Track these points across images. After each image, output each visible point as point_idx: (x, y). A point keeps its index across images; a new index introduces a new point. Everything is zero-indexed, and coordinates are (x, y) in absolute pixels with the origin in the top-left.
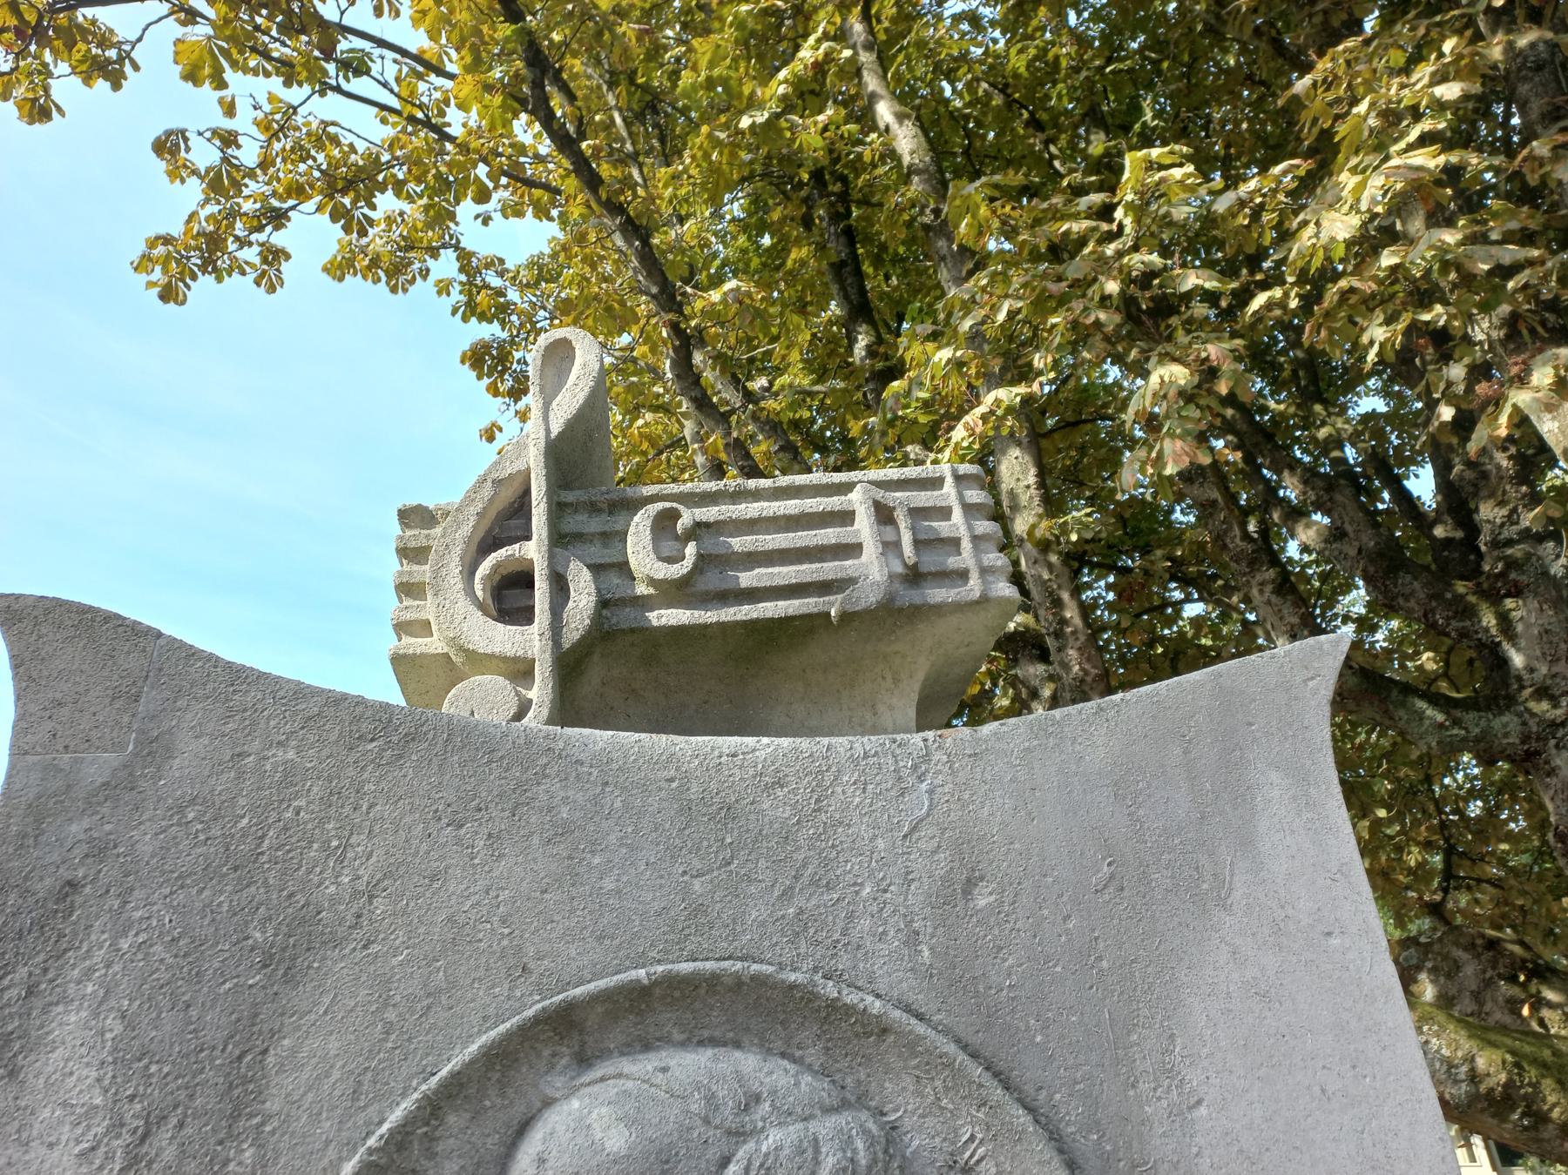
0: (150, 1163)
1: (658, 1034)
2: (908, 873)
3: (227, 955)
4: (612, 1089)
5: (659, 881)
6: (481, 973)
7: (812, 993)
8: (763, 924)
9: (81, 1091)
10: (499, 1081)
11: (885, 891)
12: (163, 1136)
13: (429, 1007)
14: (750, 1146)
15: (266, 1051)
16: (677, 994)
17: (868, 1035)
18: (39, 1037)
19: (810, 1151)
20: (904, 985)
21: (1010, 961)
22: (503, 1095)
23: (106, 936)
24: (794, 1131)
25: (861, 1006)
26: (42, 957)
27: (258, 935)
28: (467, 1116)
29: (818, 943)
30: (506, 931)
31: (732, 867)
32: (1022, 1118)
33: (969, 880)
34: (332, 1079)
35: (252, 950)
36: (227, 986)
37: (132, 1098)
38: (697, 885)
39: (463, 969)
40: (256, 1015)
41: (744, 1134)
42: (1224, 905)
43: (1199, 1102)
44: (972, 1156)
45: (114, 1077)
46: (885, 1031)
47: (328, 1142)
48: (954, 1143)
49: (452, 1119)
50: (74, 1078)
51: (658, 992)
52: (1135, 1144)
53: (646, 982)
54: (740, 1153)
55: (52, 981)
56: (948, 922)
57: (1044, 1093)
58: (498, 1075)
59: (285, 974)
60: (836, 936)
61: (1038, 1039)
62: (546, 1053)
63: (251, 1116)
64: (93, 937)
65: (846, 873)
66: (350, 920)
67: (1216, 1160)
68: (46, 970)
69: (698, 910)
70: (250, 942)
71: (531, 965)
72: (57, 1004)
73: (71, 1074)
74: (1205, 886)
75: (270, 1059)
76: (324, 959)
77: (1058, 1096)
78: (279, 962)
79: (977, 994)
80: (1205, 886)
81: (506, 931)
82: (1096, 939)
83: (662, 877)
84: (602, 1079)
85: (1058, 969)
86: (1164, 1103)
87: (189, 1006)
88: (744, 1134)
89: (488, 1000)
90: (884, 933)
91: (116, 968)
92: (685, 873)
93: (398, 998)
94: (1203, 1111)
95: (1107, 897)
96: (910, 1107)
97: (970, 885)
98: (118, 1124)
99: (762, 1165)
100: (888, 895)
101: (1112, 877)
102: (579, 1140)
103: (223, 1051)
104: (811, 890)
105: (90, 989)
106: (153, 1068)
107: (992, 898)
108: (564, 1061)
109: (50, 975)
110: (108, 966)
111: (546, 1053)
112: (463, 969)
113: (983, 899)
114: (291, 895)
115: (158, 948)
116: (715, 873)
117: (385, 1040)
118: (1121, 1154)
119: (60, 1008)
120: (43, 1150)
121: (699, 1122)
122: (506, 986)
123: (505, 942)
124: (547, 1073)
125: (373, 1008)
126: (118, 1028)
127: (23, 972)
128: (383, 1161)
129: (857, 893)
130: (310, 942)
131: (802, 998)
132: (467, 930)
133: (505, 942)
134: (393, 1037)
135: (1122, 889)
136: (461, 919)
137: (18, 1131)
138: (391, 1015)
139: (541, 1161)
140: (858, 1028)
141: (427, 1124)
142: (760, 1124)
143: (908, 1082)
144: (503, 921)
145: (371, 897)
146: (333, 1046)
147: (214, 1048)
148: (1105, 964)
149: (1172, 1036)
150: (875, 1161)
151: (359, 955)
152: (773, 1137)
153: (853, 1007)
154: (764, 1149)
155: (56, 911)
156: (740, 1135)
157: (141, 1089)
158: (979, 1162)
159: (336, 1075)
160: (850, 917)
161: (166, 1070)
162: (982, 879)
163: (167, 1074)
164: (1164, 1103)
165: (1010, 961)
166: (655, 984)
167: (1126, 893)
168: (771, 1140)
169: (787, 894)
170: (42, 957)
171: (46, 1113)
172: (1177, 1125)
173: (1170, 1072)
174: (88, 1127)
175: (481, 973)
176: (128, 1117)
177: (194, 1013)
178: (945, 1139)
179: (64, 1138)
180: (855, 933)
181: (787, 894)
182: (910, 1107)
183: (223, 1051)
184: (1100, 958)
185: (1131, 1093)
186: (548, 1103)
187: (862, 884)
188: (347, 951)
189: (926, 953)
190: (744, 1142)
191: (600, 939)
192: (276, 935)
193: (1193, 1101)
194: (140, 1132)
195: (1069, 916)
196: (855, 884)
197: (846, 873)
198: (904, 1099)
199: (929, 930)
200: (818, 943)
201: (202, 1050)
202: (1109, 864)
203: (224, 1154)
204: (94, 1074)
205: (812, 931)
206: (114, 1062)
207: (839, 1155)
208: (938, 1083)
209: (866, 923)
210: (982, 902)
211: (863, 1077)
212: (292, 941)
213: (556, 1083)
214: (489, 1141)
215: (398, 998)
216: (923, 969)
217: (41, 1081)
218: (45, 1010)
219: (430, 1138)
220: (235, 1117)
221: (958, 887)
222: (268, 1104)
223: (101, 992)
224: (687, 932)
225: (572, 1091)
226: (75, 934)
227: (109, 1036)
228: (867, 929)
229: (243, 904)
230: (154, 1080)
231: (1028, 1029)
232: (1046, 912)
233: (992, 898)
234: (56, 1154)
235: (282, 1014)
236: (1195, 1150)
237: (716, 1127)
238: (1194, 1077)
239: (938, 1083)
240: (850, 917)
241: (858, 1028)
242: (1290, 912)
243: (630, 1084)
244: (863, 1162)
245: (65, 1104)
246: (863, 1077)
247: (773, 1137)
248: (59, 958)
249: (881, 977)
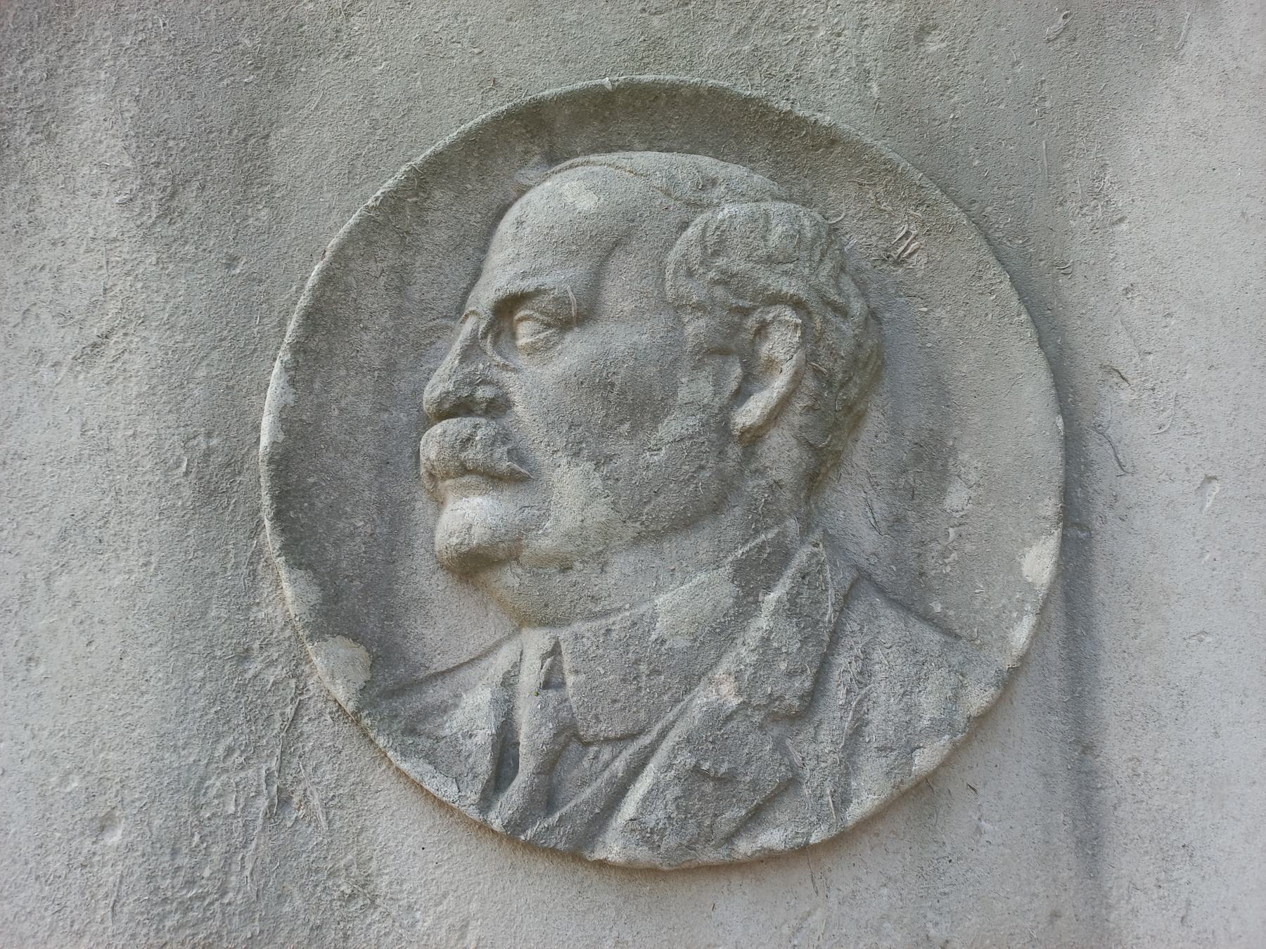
0: (181, 214)
1: (620, 143)
2: (862, 20)
3: (221, 56)
4: (580, 171)
5: (618, 16)
6: (455, 84)
7: (765, 106)
8: (719, 58)
9: (112, 156)
10: (478, 167)
11: (839, 35)
12: (189, 195)
13: (410, 110)
14: (708, 214)
15: (268, 136)
16: (638, 104)
17: (816, 148)
18: (65, 111)
19: (761, 221)
20: (852, 114)
21: (956, 99)
22: (482, 181)
23: (108, 33)
24: (746, 208)
25: (813, 119)
26: (54, 47)
27: (247, 41)
28: (452, 194)
29: (771, 76)
30: (476, 51)
31: (690, 7)
32: (957, 214)
33: (922, 28)
34: (330, 160)
35: (243, 54)
36: (225, 82)
37: (157, 164)
38: (656, 21)
39: (439, 80)
40: (254, 108)
41: (701, 206)
42: (1176, 56)
43: (1121, 220)
44: (904, 251)
45: (138, 147)
46: (833, 142)
47: (331, 209)
48: (888, 241)
49: (437, 194)
50: (104, 145)
51: (620, 99)
52: (1057, 249)
53: (609, 87)
54: (698, 220)
55: (67, 67)
56: (899, 64)
57: (976, 206)
58: (476, 162)
59: (276, 76)
60: (789, 71)
61: (976, 163)
62: (519, 149)
63: (261, 185)
64: (97, 33)
65: (801, 17)
66: (330, 33)
67: (1130, 263)
68: (61, 57)
69: (657, 43)
70: (241, 47)
71: (501, 81)
72: (76, 85)
73: (101, 142)
74: (1159, 38)
75: (272, 143)
76: (309, 66)
77: (989, 209)
78: (269, 64)
79: (921, 125)
80: (1159, 38)
81: (476, 51)
82: (1042, 82)
83: (621, 13)
84: (571, 167)
85: (1002, 107)
86: (1089, 219)
87: (193, 96)
88: (701, 206)
89: (463, 107)
90: (835, 70)
91: (123, 60)
92: (644, 10)
93: (381, 100)
94: (1124, 227)
95: (1058, 46)
96: (850, 213)
97: (923, 32)
98: (148, 185)
99: (717, 228)
100: (842, 38)
101: (1066, 28)
102: (552, 204)
103: (230, 133)
104: (767, 30)
105: (103, 76)
106: (171, 143)
107: (944, 45)
108: (536, 159)
109: (65, 62)
110: (116, 58)
111: (519, 149)
112: (439, 80)
113: (934, 45)
114: (272, 10)
115: (157, 47)
116: (673, 12)
117: (373, 134)
118: (1042, 256)
119: (80, 90)
120: (89, 198)
121: (661, 194)
122: (479, 96)
123: (476, 60)
124: (521, 167)
125: (360, 107)
126: (135, 110)
127: (39, 58)
128: (381, 218)
129: (811, 35)
130: (295, 50)
131: (756, 111)
132: (439, 48)
133: (476, 60)
134: (380, 131)
135: (1075, 40)
136: (434, 38)
137: (64, 182)
138: (376, 114)
139: (520, 223)
140: (808, 142)
141: (417, 195)
142: (716, 201)
143: (852, 189)
144: (473, 43)
145: (348, 15)
146: (327, 136)
147: (221, 131)
148: (1048, 104)
149: (1104, 166)
150: (819, 235)
151: (341, 64)
152: (727, 210)
153: (805, 120)
154: (719, 217)
155: (59, 8)
156: (696, 206)
157: (164, 158)
158: (911, 254)
159: (331, 159)
160: (803, 55)
161: (182, 145)
162: (935, 27)
163: (184, 149)
164: (1089, 219)
165: (956, 99)
166: (618, 90)
167: (1077, 44)
168: (726, 211)
169: (743, 33)
170: (54, 47)
171: (85, 170)
172: (1098, 236)
173: (1096, 195)
174: (124, 184)
175: (455, 84)
176: (156, 179)
177: (199, 102)
178: (881, 238)
179: (105, 190)
180: (808, 69)
181: (743, 33)
182: (850, 213)
183: (230, 133)
184: (1044, 99)
185: (1059, 209)
186: (522, 191)
187: (816, 28)
188: (331, 59)
189: (875, 89)
190: (702, 212)
191: (564, 62)
192: (264, 43)
193: (1115, 218)
194: (169, 190)
195: (1018, 62)
196: (809, 27)
197: (801, 17)
198: (846, 204)
199: (880, 70)
200: (771, 76)
201: (211, 132)
202: (1065, 17)
203: (243, 211)
204: (121, 144)
205: (766, 66)
206: (137, 136)
207: (788, 226)
208: (880, 189)
209: (818, 62)
210: (932, 48)
211: (808, 186)
212: (278, 48)
213: (528, 174)
214: (472, 218)
215: (381, 100)
216: (872, 101)
217: (76, 145)
218: (67, 89)
219: (420, 208)
220: (247, 184)
221: (912, 34)
222: (275, 177)
223: (114, 79)
224: (646, 60)
225: (546, 178)
226: (81, 30)
227: (126, 115)
228: (819, 66)
229: (229, 15)
230: (174, 152)
231: (967, 154)
232: (995, 58)
233: (944, 45)
234: (100, 201)
235: (278, 108)
236: (1111, 256)
237: (676, 199)
238: (1120, 200)
239: (880, 189)
240: (803, 55)
241: (808, 142)
242: (1242, 63)
243: (596, 169)
244: (809, 235)
245: (100, 165)
246: (808, 186)
247: (727, 210)
248: (69, 48)
249: (832, 107)
